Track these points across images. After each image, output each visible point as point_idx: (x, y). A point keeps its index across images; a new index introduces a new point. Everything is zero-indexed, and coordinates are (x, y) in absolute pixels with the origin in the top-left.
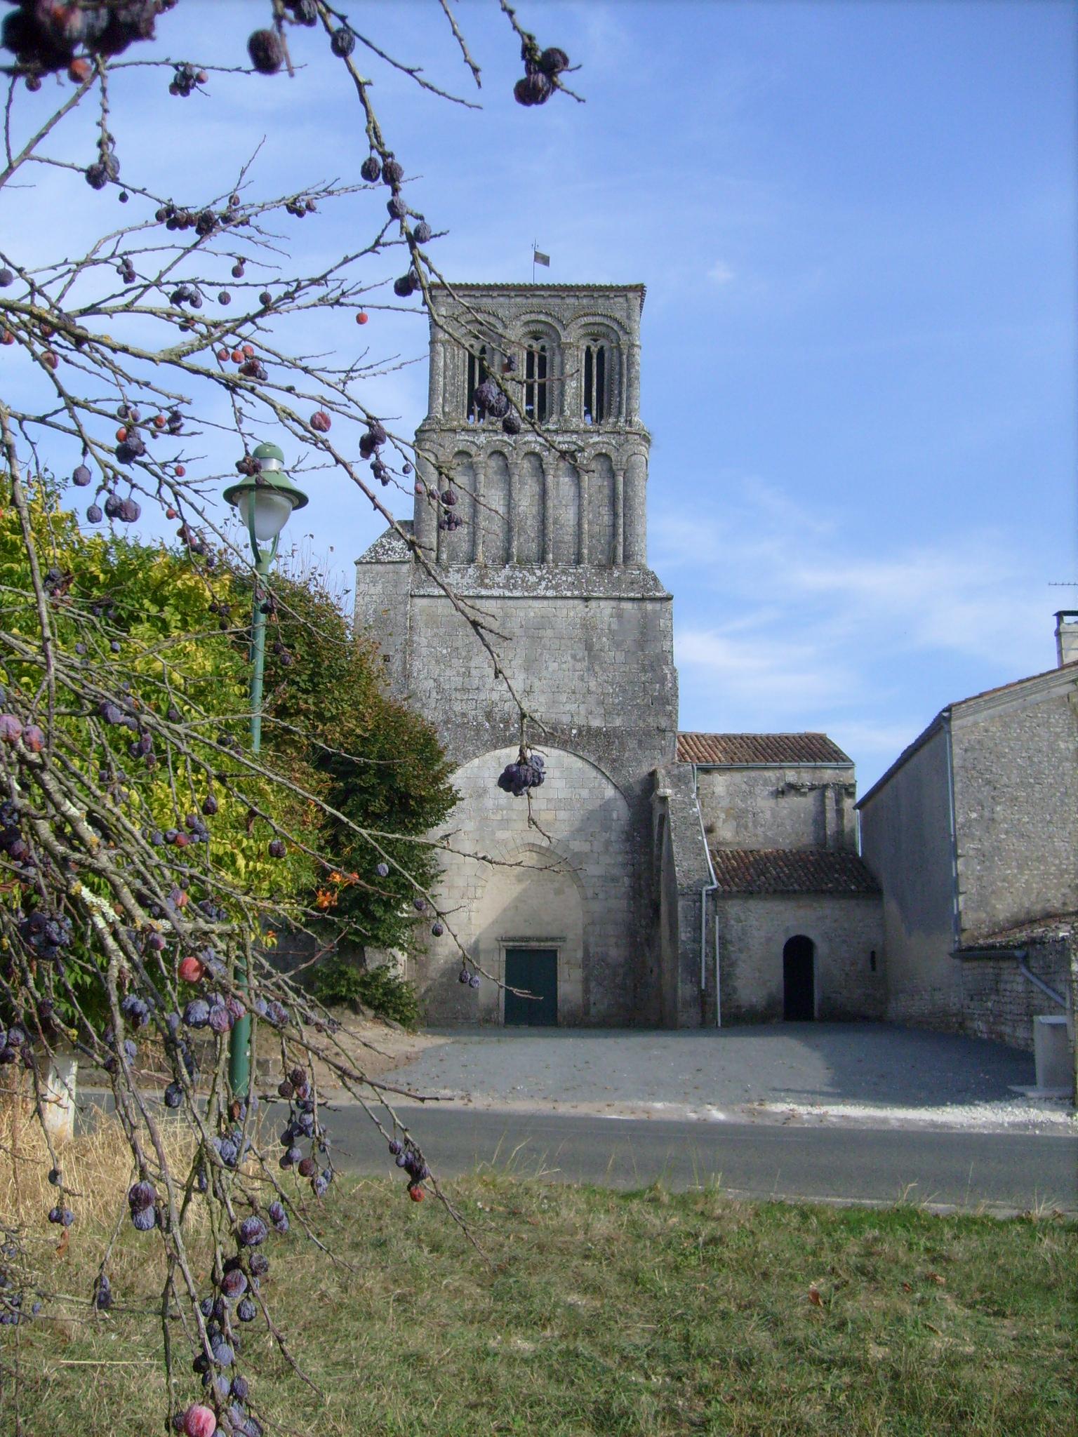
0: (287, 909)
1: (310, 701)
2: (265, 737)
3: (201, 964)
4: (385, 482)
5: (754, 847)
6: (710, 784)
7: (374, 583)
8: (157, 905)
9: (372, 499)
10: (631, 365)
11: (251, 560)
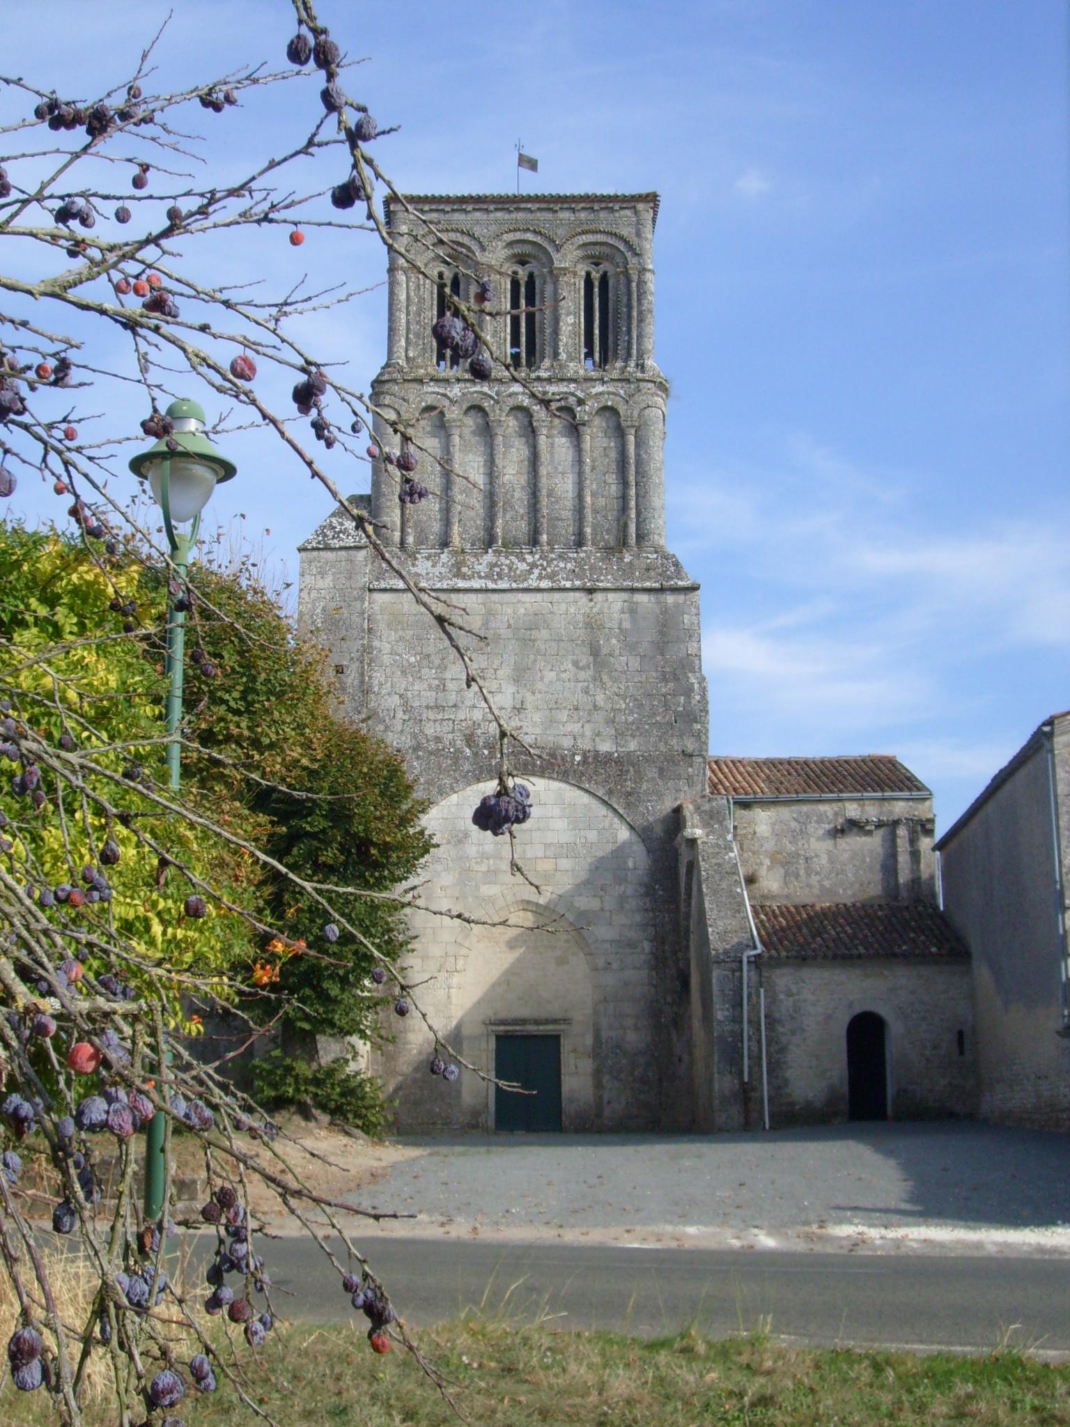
0: (219, 988)
1: (243, 725)
2: (186, 772)
3: (97, 1050)
4: (329, 444)
5: (809, 901)
6: (752, 822)
7: (322, 574)
8: (45, 980)
9: (310, 464)
10: (641, 295)
11: (165, 546)
